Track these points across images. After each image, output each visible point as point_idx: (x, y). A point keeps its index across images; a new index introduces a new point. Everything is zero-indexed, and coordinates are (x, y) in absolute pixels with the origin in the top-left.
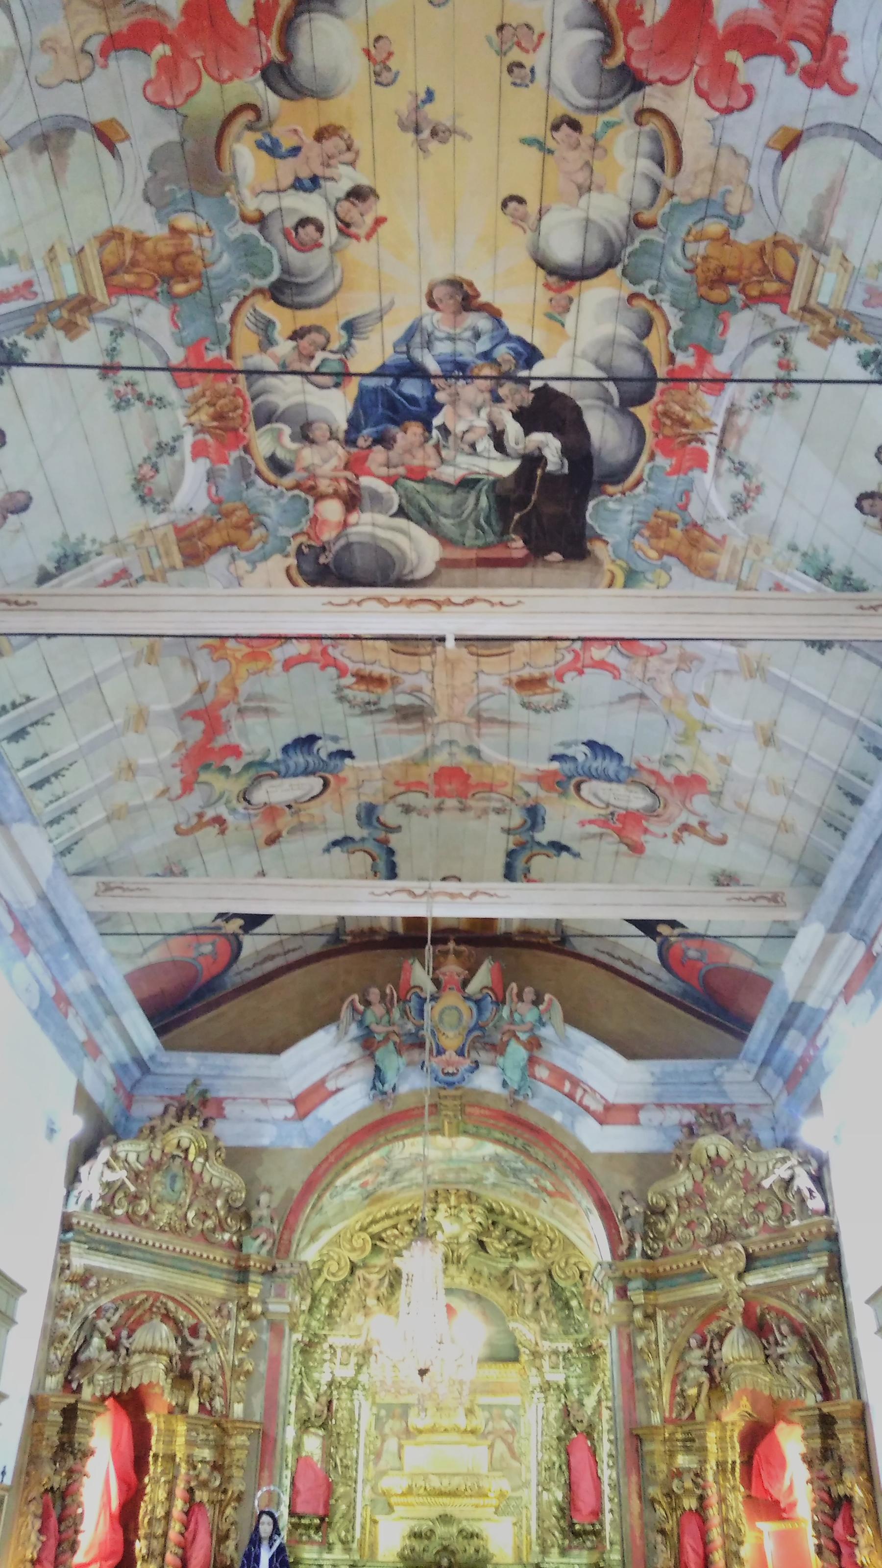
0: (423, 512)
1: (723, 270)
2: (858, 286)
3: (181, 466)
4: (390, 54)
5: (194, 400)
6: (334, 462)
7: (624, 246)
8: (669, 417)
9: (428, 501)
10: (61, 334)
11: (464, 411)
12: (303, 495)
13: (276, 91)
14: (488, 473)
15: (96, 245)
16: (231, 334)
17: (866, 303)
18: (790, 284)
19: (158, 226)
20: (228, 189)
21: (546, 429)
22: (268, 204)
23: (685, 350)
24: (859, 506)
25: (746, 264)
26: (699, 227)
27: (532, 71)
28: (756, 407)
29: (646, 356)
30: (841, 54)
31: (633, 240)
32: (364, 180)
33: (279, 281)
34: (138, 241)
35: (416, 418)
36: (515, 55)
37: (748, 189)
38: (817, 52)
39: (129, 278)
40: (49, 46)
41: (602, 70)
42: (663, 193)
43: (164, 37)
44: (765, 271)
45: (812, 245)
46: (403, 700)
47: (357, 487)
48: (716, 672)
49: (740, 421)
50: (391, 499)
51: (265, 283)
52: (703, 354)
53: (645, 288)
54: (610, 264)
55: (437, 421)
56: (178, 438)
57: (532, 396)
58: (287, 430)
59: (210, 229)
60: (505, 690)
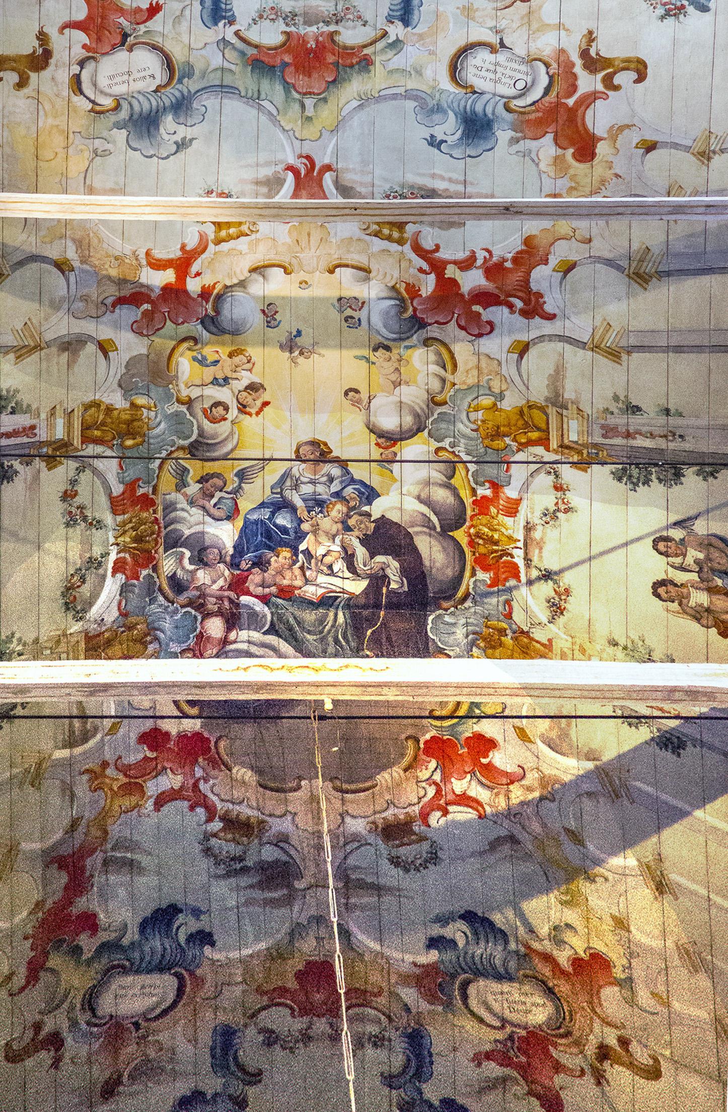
0: (291, 629)
1: (498, 427)
2: (595, 426)
3: (104, 577)
4: (277, 312)
5: (124, 524)
6: (221, 582)
7: (428, 418)
8: (481, 538)
9: (295, 618)
10: (43, 464)
11: (323, 539)
12: (193, 612)
13: (208, 331)
14: (344, 591)
15: (81, 409)
16: (158, 476)
17: (604, 436)
18: (547, 431)
19: (124, 402)
20: (171, 383)
21: (386, 553)
22: (195, 393)
23: (482, 484)
24: (656, 594)
25: (513, 422)
26: (475, 402)
27: (359, 320)
28: (547, 523)
29: (454, 491)
30: (541, 300)
31: (433, 415)
32: (257, 380)
33: (196, 441)
34: (109, 410)
35: (286, 545)
36: (349, 312)
37: (503, 378)
38: (526, 302)
39: (97, 433)
40: (85, 299)
41: (400, 319)
42: (448, 385)
43: (148, 299)
44: (526, 425)
45: (554, 404)
46: (269, 853)
47: (238, 605)
48: (580, 796)
49: (537, 534)
50: (265, 616)
51: (186, 443)
52: (496, 486)
53: (446, 443)
54: (420, 430)
55: (302, 547)
56: (106, 555)
57: (373, 525)
58: (188, 554)
59: (155, 406)
60: (371, 839)
